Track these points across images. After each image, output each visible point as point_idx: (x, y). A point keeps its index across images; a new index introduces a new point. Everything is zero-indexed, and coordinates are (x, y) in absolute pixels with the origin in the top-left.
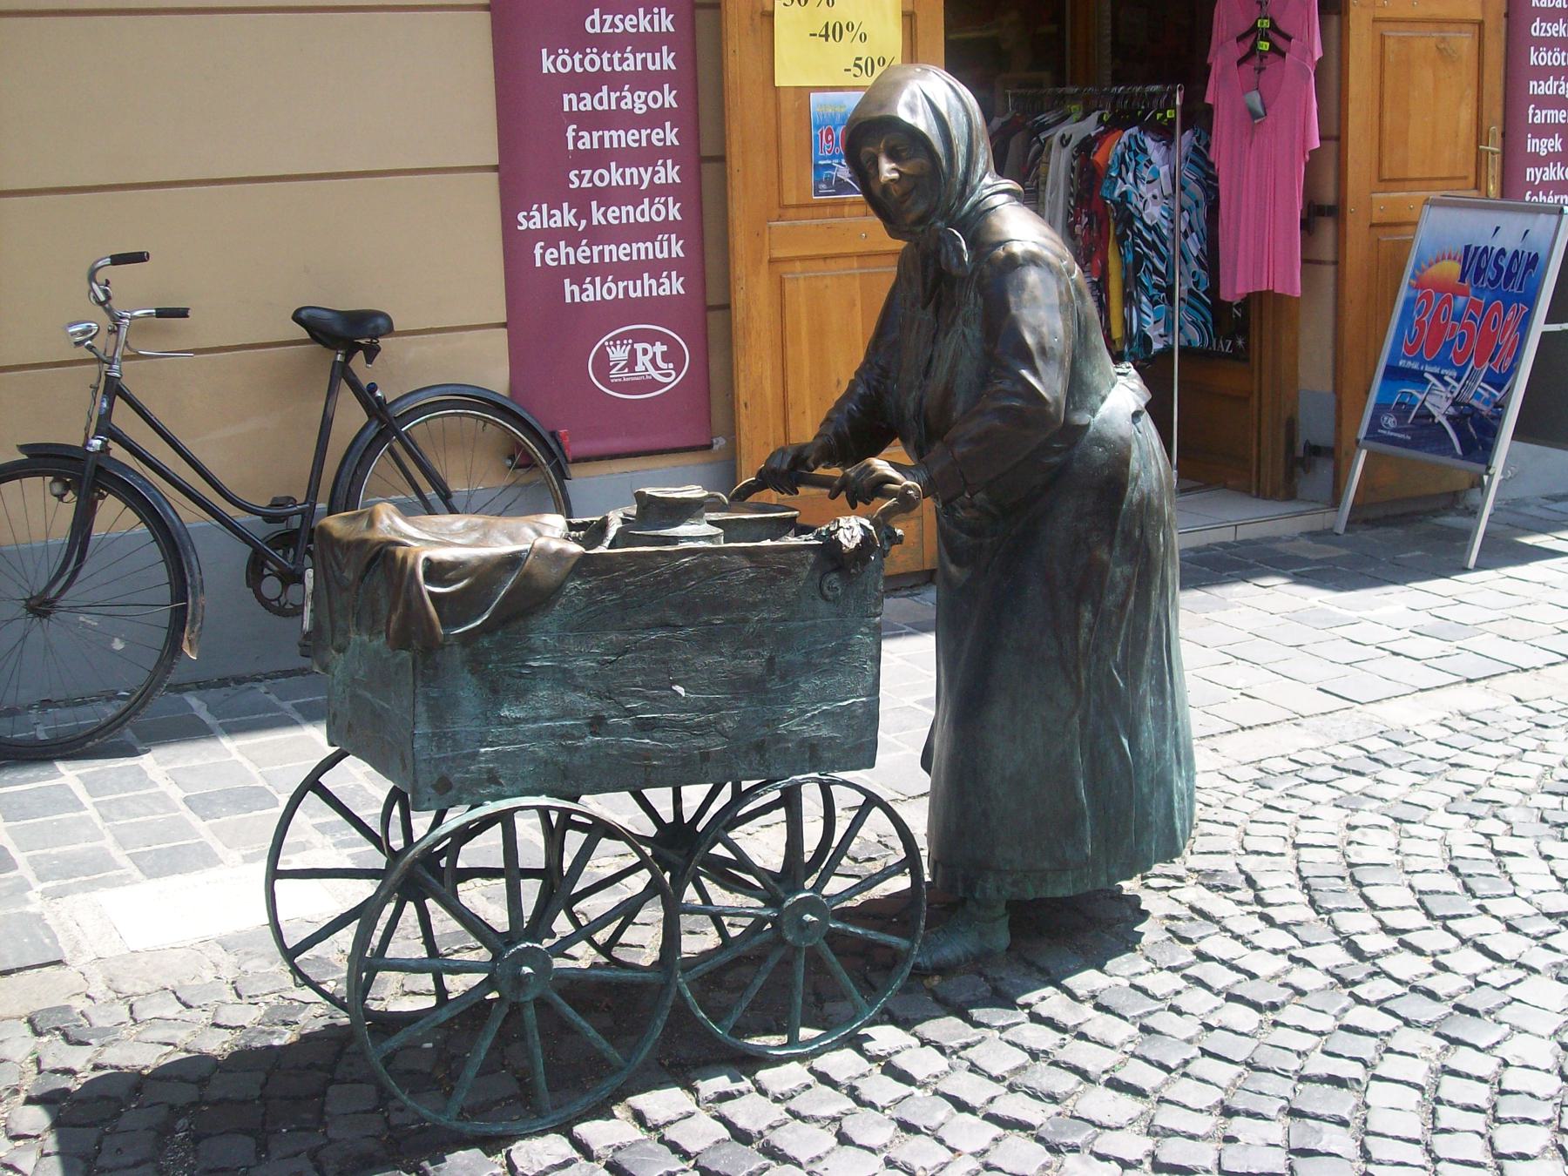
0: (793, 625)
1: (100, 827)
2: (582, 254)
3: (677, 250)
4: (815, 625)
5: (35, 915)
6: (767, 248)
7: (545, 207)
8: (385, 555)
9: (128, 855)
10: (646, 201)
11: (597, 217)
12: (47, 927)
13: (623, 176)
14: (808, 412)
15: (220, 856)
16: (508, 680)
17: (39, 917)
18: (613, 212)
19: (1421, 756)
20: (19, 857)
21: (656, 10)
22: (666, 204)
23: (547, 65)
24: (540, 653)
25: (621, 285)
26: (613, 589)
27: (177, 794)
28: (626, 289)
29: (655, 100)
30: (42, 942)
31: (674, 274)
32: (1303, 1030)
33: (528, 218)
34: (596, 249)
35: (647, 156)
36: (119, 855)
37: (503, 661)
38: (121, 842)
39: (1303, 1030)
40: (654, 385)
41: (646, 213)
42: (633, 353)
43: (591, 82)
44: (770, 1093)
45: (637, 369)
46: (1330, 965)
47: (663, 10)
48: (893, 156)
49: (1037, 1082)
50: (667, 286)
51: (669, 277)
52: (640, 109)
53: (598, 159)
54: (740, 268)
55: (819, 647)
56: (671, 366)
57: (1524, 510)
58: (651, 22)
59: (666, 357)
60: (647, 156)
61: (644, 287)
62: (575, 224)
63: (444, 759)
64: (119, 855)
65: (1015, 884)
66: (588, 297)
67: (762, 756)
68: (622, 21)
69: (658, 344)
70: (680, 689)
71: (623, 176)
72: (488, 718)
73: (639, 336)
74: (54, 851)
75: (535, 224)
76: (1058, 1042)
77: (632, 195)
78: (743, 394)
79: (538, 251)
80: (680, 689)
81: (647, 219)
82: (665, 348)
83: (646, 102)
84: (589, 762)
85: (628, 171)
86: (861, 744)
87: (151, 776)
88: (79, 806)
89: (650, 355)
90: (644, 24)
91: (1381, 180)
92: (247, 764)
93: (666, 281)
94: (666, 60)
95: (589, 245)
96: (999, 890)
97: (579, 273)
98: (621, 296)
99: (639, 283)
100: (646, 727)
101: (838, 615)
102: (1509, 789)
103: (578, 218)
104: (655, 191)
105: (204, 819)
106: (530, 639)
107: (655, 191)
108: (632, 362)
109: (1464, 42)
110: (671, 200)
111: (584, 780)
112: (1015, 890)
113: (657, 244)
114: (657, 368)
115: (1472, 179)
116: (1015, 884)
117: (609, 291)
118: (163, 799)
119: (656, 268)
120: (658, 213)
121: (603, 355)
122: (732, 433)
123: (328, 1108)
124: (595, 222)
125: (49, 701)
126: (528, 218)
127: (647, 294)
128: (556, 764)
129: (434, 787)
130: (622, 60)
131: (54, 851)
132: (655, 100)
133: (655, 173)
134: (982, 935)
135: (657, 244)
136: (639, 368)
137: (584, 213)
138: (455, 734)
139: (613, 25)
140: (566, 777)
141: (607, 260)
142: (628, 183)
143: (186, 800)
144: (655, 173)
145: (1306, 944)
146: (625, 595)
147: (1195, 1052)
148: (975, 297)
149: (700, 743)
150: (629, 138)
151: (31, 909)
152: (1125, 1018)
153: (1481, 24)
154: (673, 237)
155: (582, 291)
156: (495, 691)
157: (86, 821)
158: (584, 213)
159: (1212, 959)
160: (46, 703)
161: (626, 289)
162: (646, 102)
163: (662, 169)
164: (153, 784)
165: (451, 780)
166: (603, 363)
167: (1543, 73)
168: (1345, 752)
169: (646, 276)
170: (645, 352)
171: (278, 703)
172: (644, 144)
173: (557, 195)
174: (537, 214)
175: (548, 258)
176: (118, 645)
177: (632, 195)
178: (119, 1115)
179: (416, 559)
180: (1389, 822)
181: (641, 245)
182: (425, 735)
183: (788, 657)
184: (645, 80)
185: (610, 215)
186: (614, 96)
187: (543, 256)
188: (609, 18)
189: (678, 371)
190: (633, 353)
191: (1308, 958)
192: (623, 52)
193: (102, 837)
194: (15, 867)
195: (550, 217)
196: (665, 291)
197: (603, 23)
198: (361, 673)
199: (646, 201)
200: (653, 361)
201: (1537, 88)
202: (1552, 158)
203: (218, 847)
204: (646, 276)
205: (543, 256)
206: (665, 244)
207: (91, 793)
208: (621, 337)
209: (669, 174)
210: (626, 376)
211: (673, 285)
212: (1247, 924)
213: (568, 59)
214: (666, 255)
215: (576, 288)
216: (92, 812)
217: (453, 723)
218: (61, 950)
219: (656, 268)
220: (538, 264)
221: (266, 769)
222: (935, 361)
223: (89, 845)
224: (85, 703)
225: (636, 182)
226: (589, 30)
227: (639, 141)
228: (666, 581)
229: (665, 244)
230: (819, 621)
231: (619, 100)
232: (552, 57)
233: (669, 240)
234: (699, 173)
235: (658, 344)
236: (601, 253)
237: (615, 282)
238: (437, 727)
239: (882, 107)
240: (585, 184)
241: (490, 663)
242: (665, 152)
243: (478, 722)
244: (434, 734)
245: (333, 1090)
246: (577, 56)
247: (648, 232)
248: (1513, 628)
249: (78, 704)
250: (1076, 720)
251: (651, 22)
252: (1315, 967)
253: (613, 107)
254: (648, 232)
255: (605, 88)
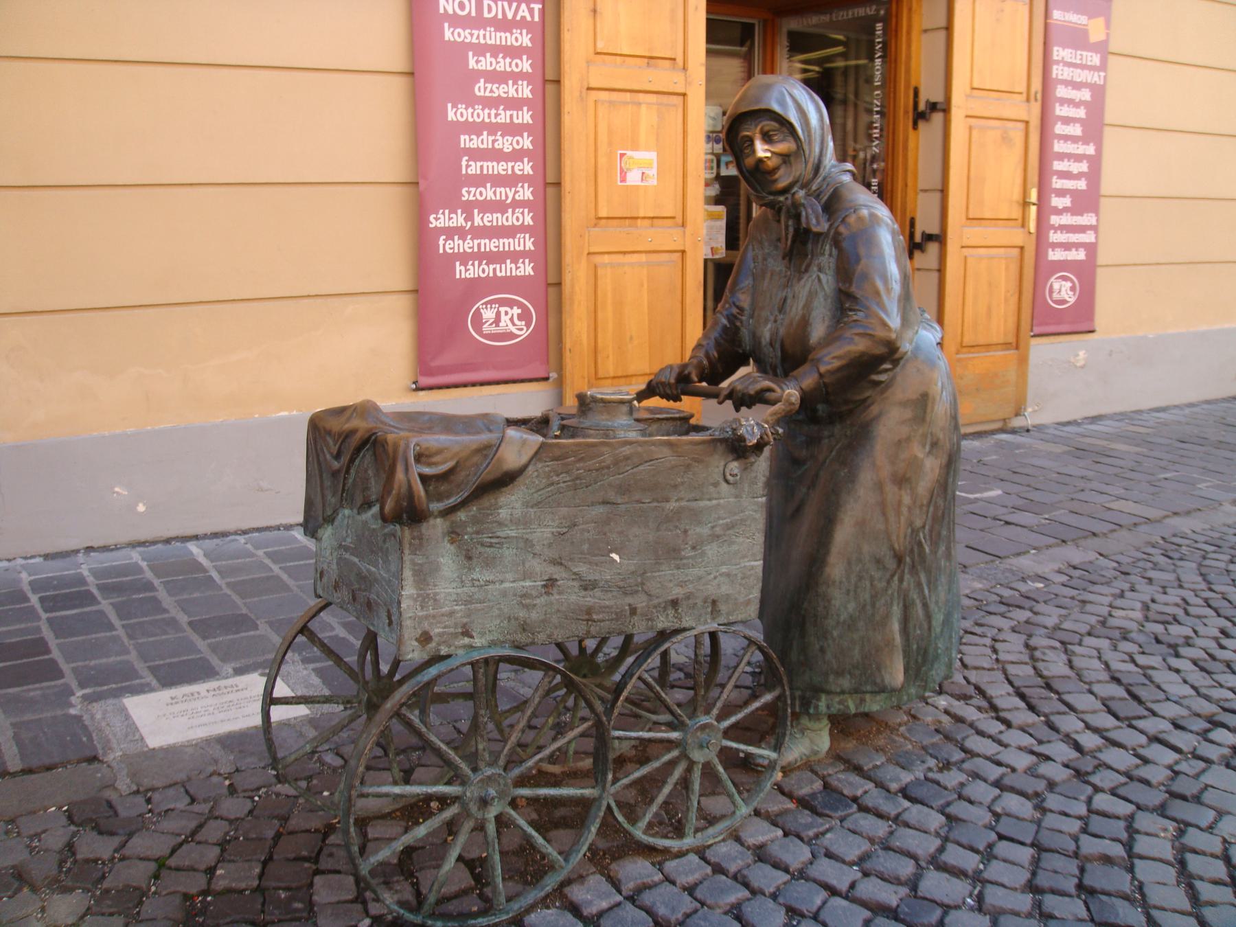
0: (702, 504)
1: (127, 644)
2: (468, 245)
3: (529, 245)
4: (718, 505)
5: (75, 717)
6: (586, 245)
7: (447, 211)
8: (375, 440)
9: (149, 667)
10: (510, 210)
11: (477, 221)
12: (85, 727)
13: (495, 193)
14: (611, 357)
15: (217, 669)
16: (480, 549)
17: (78, 718)
18: (487, 217)
19: (1056, 595)
20: (65, 667)
21: (520, 82)
22: (523, 213)
23: (451, 116)
24: (506, 526)
25: (492, 267)
26: (566, 472)
27: (183, 619)
28: (495, 270)
29: (518, 143)
30: (81, 740)
31: (527, 261)
32: (1066, 815)
33: (437, 219)
34: (476, 242)
35: (511, 181)
36: (140, 666)
37: (477, 533)
38: (144, 657)
39: (1066, 815)
40: (511, 336)
41: (509, 219)
42: (498, 314)
43: (475, 129)
44: (678, 882)
45: (501, 324)
46: (1065, 759)
47: (525, 83)
48: (767, 138)
49: (883, 866)
50: (522, 269)
51: (524, 263)
52: (508, 149)
53: (479, 181)
54: (568, 258)
55: (721, 522)
56: (523, 323)
57: (1046, 431)
58: (517, 90)
59: (520, 317)
60: (511, 181)
61: (507, 269)
62: (464, 224)
63: (427, 617)
64: (140, 666)
65: (840, 703)
66: (470, 275)
67: (676, 610)
68: (498, 88)
69: (515, 308)
70: (615, 557)
71: (495, 193)
72: (462, 582)
73: (502, 302)
74: (93, 663)
75: (441, 223)
76: (887, 829)
77: (499, 207)
78: (568, 343)
79: (441, 242)
80: (615, 557)
81: (510, 223)
82: (519, 311)
83: (511, 144)
84: (542, 617)
85: (498, 190)
86: (749, 600)
87: (165, 605)
88: (111, 627)
89: (510, 316)
90: (512, 93)
91: (968, 219)
92: (235, 597)
93: (522, 265)
94: (525, 117)
95: (472, 239)
96: (828, 707)
97: (465, 258)
98: (491, 275)
99: (503, 266)
100: (588, 586)
101: (736, 497)
102: (1123, 618)
103: (466, 220)
104: (516, 204)
105: (204, 638)
106: (499, 514)
107: (516, 204)
108: (497, 320)
109: (1017, 133)
110: (526, 210)
111: (539, 632)
112: (841, 707)
113: (517, 240)
114: (514, 324)
115: (1020, 221)
116: (840, 703)
117: (484, 271)
118: (173, 623)
119: (515, 256)
120: (518, 219)
121: (478, 314)
122: (560, 368)
123: (315, 898)
124: (476, 224)
125: (92, 547)
126: (437, 219)
127: (508, 274)
128: (517, 619)
129: (417, 640)
130: (497, 115)
131: (93, 663)
132: (518, 143)
133: (516, 192)
134: (812, 741)
135: (517, 240)
136: (502, 324)
137: (469, 218)
138: (436, 594)
139: (491, 91)
140: (524, 630)
141: (483, 250)
142: (498, 198)
143: (190, 623)
144: (516, 192)
145: (1040, 742)
146: (577, 478)
147: (993, 836)
148: (831, 250)
149: (629, 600)
150: (501, 168)
151: (73, 711)
152: (932, 808)
153: (1027, 122)
154: (527, 236)
155: (467, 270)
156: (469, 558)
157: (116, 639)
158: (469, 218)
159: (978, 755)
160: (90, 549)
161: (495, 270)
162: (511, 144)
163: (521, 190)
164: (166, 611)
165: (432, 634)
166: (478, 320)
167: (1062, 156)
168: (1006, 593)
169: (508, 261)
170: (506, 313)
171: (254, 551)
172: (510, 172)
173: (454, 203)
174: (442, 216)
175: (447, 247)
176: (141, 508)
177: (499, 207)
178: (140, 903)
179: (407, 446)
180: (1058, 645)
181: (505, 240)
182: (411, 597)
183: (698, 530)
184: (512, 129)
185: (485, 219)
186: (491, 138)
187: (444, 245)
188: (489, 86)
189: (528, 326)
190: (498, 314)
191: (1047, 753)
192: (497, 109)
193: (128, 653)
194: (63, 677)
195: (450, 219)
196: (520, 273)
197: (485, 89)
198: (349, 540)
199: (510, 210)
200: (512, 320)
201: (1058, 166)
202: (1065, 210)
203: (215, 661)
204: (508, 261)
205: (444, 245)
206: (522, 241)
207: (121, 618)
208: (491, 302)
209: (526, 193)
210: (493, 329)
211: (526, 269)
212: (995, 727)
213: (464, 111)
214: (522, 248)
215: (463, 268)
216: (121, 632)
217: (435, 586)
218: (95, 748)
219: (515, 256)
220: (441, 251)
221: (248, 600)
222: (789, 301)
223: (119, 658)
224: (117, 549)
225: (504, 198)
226: (478, 93)
227: (507, 170)
228: (608, 467)
229: (522, 241)
230: (722, 501)
231: (494, 142)
232: (454, 110)
233: (524, 238)
234: (545, 191)
235: (515, 308)
236: (479, 245)
237: (487, 264)
238: (421, 589)
239: (758, 100)
240: (471, 198)
241: (466, 534)
242: (523, 178)
243: (454, 585)
244: (419, 595)
245: (318, 880)
246: (470, 110)
247: (510, 232)
248: (1076, 506)
249: (112, 550)
250: (896, 578)
251: (517, 90)
252: (1054, 761)
253: (490, 146)
254: (510, 232)
255: (485, 133)
